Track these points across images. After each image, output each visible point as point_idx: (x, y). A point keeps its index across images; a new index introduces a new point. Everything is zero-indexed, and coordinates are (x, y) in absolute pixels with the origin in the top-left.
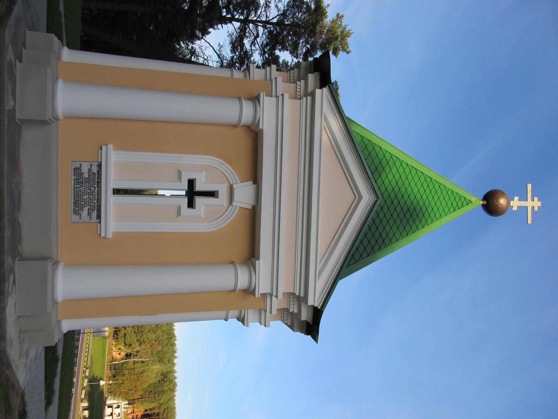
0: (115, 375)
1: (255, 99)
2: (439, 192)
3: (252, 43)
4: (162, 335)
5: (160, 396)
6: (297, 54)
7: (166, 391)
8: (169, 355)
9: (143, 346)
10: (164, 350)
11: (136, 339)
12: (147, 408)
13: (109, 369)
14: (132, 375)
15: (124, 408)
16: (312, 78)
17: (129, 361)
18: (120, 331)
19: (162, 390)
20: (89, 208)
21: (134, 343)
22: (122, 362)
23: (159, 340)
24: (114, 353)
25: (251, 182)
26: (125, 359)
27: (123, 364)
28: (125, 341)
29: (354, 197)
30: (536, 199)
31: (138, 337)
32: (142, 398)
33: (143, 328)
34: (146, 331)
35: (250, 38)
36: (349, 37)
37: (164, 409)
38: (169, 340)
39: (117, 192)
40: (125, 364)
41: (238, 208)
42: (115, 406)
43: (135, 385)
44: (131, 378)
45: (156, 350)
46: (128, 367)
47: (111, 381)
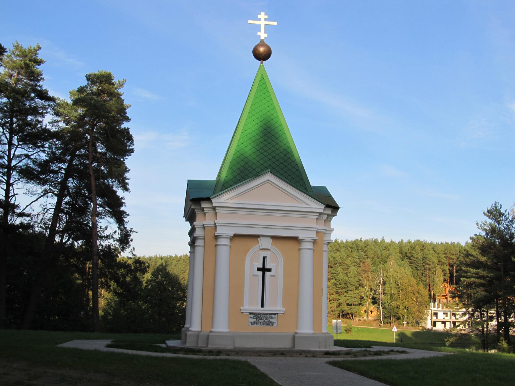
0: (397, 317)
1: (216, 237)
4: (353, 259)
5: (429, 263)
7: (424, 255)
8: (378, 250)
9: (364, 282)
10: (372, 256)
11: (354, 291)
12: (442, 279)
13: (389, 324)
14: (399, 297)
16: (204, 205)
17: (381, 301)
18: (343, 310)
19: (421, 260)
21: (360, 294)
22: (382, 309)
23: (358, 262)
24: (370, 318)
25: (259, 239)
26: (379, 305)
27: (384, 308)
28: (356, 305)
29: (268, 183)
30: (259, 16)
31: (353, 288)
32: (429, 286)
33: (342, 282)
34: (346, 278)
38: (360, 248)
40: (385, 305)
41: (272, 246)
42: (434, 318)
43: (412, 294)
44: (402, 298)
45: (371, 266)
46: (389, 302)
47: (404, 322)
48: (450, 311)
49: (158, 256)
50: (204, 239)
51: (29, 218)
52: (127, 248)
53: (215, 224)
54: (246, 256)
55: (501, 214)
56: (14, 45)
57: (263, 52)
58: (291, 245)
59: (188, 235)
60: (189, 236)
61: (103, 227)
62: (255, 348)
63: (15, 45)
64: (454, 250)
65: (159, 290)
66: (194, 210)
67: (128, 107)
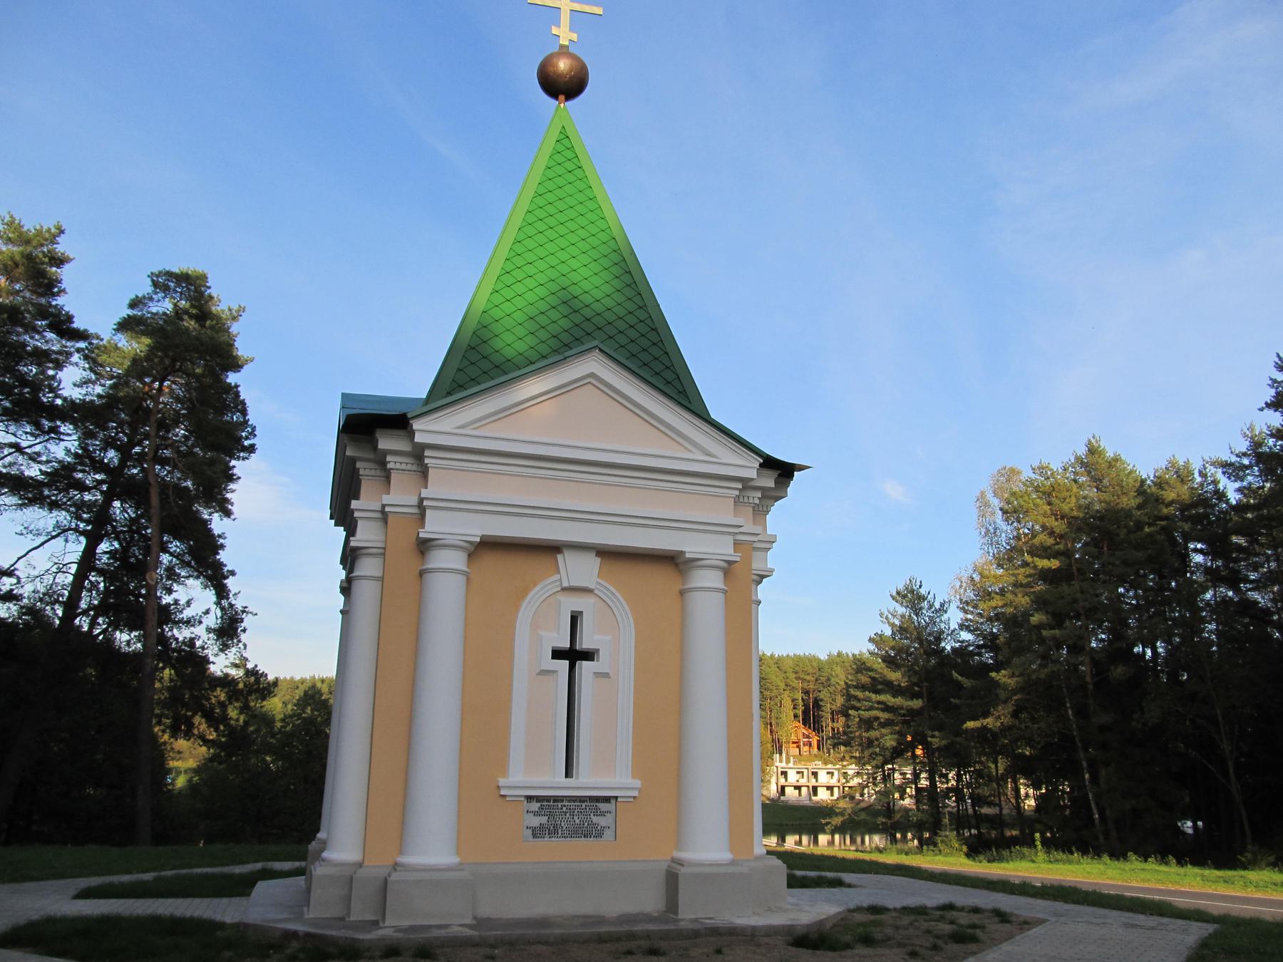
1: (424, 546)
2: (550, 197)
3: (34, 460)
5: (771, 687)
6: (59, 353)
15: (788, 761)
16: (386, 442)
20: (594, 815)
25: (560, 557)
29: (590, 386)
35: (22, 465)
36: (22, 224)
37: (798, 678)
39: (568, 774)
42: (782, 781)
48: (807, 769)
49: (317, 677)
50: (384, 554)
51: (14, 581)
52: (233, 647)
53: (421, 500)
54: (517, 607)
55: (922, 598)
56: (3, 220)
57: (565, 72)
58: (659, 577)
59: (341, 563)
60: (342, 566)
61: (182, 602)
62: (543, 922)
63: (5, 221)
64: (810, 667)
65: (306, 734)
66: (353, 461)
67: (247, 361)
